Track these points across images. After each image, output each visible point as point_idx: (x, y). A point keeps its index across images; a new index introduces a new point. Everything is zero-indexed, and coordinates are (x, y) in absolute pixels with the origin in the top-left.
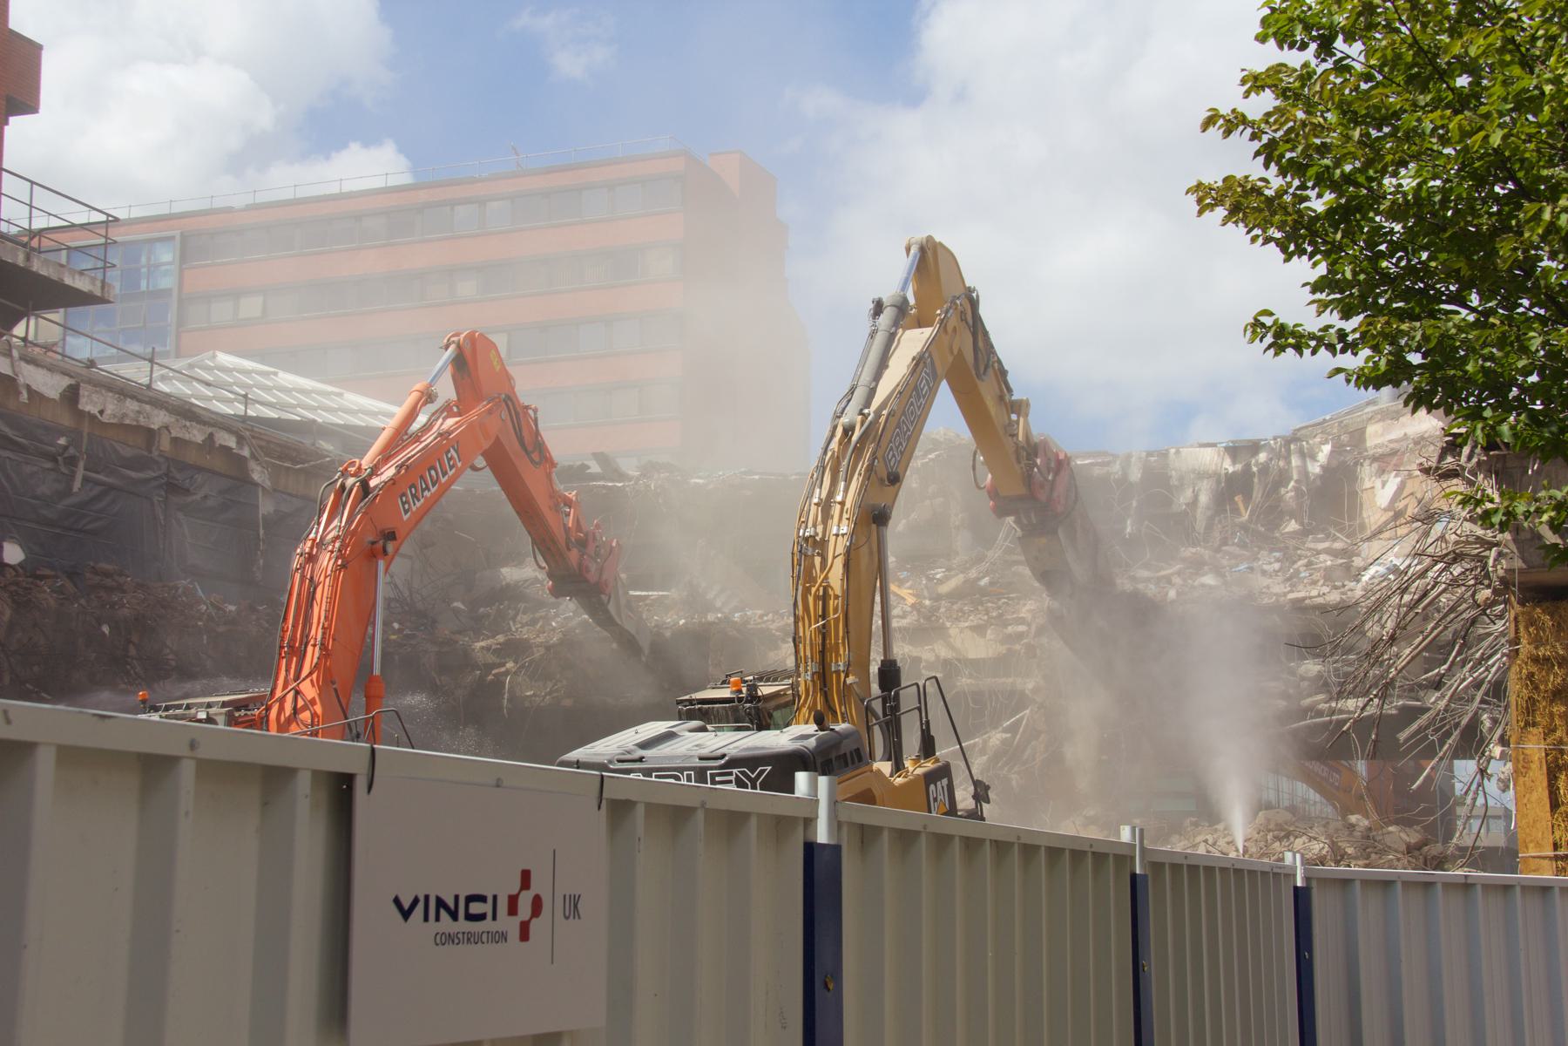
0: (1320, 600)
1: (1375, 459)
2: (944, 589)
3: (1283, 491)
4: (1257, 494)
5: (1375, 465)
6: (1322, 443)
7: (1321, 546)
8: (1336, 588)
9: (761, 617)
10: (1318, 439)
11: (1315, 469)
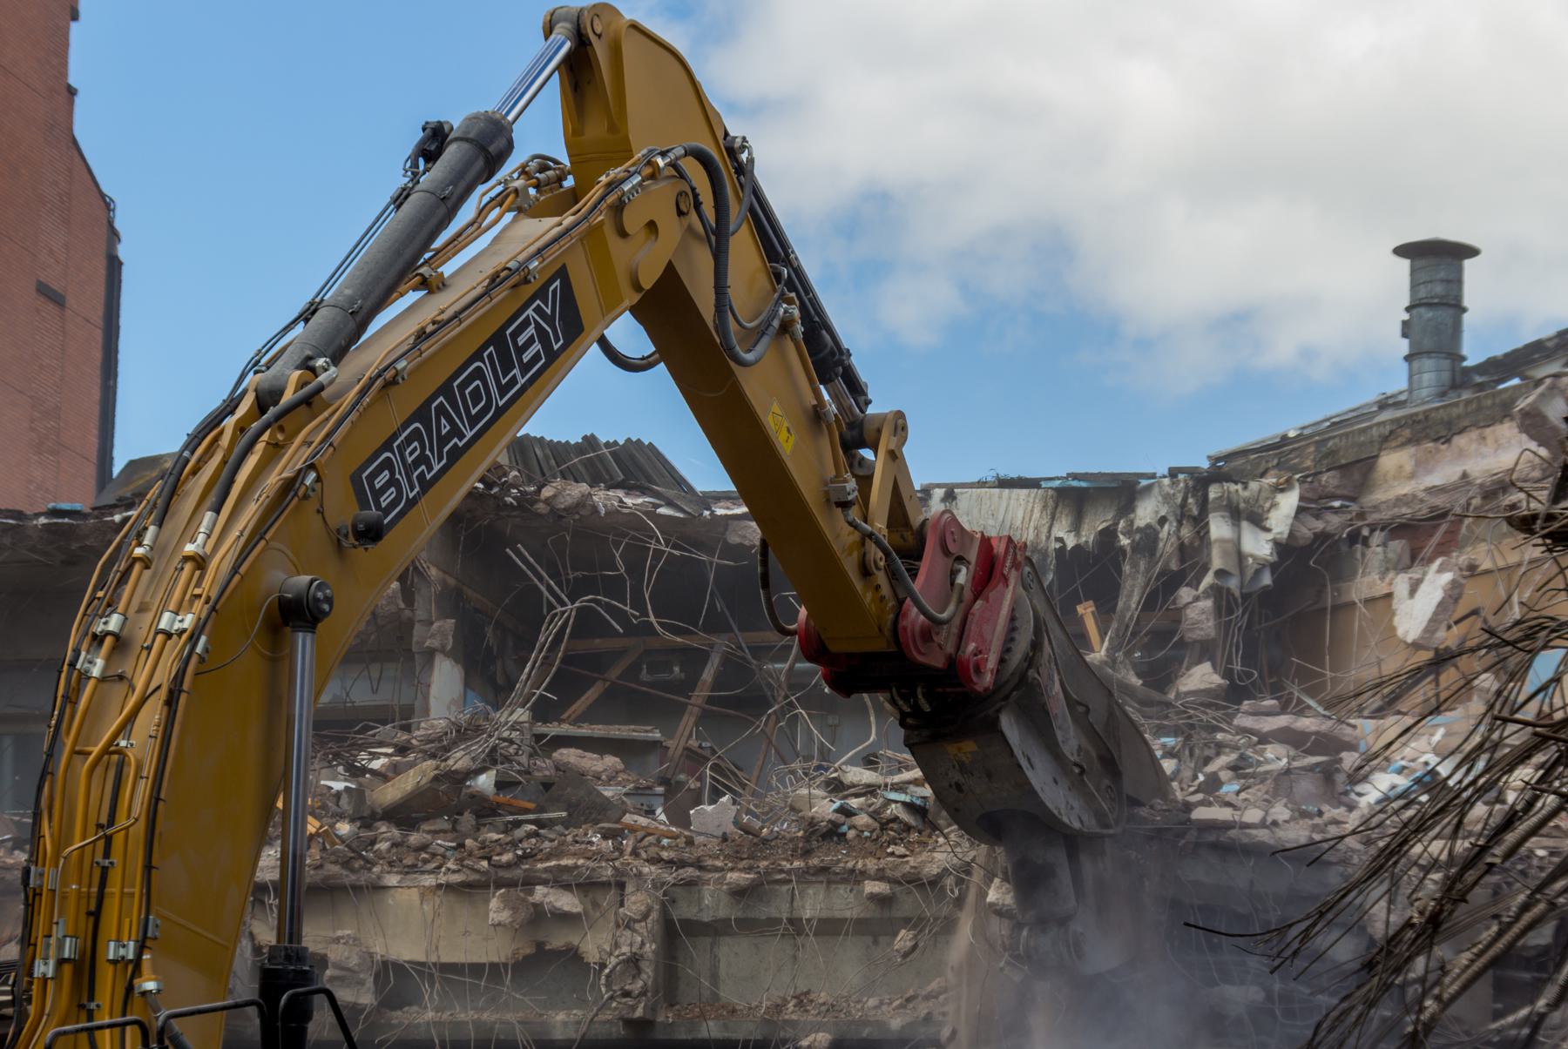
0: (1263, 835)
2: (390, 793)
3: (1185, 594)
4: (1131, 596)
5: (1397, 546)
6: (1279, 489)
7: (1270, 724)
8: (1305, 815)
10: (1270, 480)
11: (1258, 546)
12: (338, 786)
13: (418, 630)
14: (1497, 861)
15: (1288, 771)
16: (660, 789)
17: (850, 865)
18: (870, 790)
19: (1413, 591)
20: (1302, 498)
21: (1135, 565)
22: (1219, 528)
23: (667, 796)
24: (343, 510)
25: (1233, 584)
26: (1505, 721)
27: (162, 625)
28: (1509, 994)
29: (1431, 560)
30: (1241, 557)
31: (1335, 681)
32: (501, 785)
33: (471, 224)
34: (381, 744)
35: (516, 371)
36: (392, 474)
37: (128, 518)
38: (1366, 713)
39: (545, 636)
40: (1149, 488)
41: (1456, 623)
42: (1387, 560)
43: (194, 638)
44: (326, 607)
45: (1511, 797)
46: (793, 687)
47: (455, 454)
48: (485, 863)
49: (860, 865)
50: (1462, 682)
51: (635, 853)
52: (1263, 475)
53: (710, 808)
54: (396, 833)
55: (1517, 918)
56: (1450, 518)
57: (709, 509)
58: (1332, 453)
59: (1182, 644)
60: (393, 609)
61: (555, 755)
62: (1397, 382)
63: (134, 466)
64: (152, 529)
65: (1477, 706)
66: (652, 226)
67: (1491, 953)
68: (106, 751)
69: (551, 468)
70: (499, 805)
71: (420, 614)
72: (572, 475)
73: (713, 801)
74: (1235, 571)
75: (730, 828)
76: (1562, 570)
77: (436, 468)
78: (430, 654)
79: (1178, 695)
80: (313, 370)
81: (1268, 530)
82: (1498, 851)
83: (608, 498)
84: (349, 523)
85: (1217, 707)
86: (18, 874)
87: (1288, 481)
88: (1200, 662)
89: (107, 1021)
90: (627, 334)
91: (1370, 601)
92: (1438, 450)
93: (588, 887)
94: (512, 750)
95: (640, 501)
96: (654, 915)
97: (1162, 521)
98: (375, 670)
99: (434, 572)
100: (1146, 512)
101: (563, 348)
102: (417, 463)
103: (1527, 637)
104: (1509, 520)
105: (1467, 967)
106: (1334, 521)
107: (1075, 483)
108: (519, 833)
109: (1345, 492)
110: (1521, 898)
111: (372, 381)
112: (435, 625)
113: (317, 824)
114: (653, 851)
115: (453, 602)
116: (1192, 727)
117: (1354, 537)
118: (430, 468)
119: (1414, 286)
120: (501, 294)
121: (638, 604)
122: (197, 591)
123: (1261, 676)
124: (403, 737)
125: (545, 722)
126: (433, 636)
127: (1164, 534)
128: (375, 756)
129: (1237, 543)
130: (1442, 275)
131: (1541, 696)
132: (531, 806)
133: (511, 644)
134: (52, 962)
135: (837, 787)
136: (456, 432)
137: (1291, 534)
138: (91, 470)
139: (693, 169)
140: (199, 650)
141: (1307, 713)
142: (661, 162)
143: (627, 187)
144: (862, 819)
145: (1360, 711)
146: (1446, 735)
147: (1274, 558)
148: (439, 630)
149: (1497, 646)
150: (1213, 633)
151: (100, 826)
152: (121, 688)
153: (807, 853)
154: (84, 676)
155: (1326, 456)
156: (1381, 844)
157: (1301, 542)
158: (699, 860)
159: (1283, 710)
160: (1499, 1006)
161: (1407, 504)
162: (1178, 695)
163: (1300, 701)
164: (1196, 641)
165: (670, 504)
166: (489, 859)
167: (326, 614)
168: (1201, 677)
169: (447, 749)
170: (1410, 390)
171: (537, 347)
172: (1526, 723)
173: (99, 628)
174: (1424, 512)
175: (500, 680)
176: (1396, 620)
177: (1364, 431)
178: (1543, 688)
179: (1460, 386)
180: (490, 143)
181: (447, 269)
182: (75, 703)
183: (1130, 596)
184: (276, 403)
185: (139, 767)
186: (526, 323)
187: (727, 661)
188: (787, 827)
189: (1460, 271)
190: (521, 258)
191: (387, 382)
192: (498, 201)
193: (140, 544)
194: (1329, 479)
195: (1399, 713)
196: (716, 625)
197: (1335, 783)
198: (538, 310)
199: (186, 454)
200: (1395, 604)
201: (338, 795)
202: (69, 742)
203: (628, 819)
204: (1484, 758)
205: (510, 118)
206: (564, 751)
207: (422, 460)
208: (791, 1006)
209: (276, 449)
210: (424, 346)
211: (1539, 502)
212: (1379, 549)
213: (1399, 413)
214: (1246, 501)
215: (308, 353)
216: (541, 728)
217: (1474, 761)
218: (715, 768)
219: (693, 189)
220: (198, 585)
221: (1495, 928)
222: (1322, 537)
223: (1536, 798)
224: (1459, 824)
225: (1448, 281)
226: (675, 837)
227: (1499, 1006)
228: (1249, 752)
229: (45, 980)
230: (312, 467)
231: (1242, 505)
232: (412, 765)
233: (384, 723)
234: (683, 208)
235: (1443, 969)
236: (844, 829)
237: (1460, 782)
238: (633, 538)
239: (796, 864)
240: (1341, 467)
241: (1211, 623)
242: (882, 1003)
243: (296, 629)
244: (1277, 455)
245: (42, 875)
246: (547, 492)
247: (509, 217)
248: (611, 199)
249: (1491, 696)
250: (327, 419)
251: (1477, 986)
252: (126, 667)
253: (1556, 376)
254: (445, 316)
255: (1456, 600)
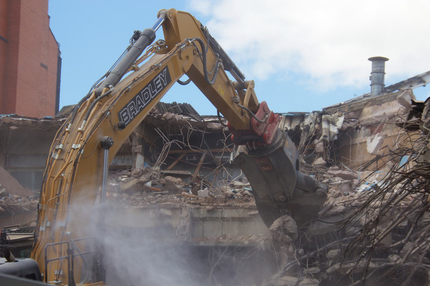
1: (368, 126)
3: (316, 141)
5: (368, 130)
6: (339, 116)
9: (17, 199)
10: (337, 114)
11: (334, 130)
12: (114, 185)
13: (133, 148)
14: (393, 206)
15: (341, 184)
16: (191, 186)
17: (236, 205)
18: (241, 187)
19: (371, 141)
20: (345, 119)
21: (304, 134)
22: (324, 125)
23: (192, 188)
24: (116, 121)
25: (328, 139)
26: (395, 172)
27: (73, 147)
28: (396, 239)
29: (376, 134)
30: (330, 132)
31: (352, 162)
32: (153, 185)
33: (145, 55)
34: (124, 175)
35: (156, 90)
36: (127, 113)
37: (65, 120)
38: (360, 170)
39: (164, 150)
40: (308, 116)
41: (382, 149)
42: (365, 133)
43: (80, 150)
44: (112, 144)
45: (395, 191)
46: (222, 162)
47: (142, 109)
48: (149, 203)
49: (238, 205)
50: (383, 164)
51: (184, 201)
52: (335, 113)
53: (202, 191)
54: (127, 196)
55: (397, 220)
56: (381, 123)
57: (203, 119)
58: (352, 108)
59: (316, 153)
60: (127, 143)
61: (166, 178)
62: (368, 90)
63: (65, 108)
64: (70, 124)
65: (387, 169)
66: (187, 57)
67: (391, 228)
68: (59, 177)
69: (165, 109)
70: (152, 190)
71: (134, 144)
72: (170, 111)
73: (203, 189)
74: (328, 136)
75: (207, 196)
76: (409, 136)
77: (137, 112)
78: (136, 153)
79: (314, 165)
80: (109, 88)
81: (336, 126)
82: (393, 204)
83: (179, 117)
84: (117, 124)
85: (324, 168)
86: (36, 206)
87: (341, 114)
88: (319, 157)
89: (58, 242)
90: (184, 78)
91: (361, 143)
92: (378, 107)
93: (173, 209)
94: (155, 176)
95: (186, 118)
96: (189, 216)
97: (311, 124)
98: (123, 157)
99: (137, 134)
100: (307, 121)
101: (167, 85)
102: (133, 111)
103: (401, 152)
104: (397, 124)
105: (385, 232)
106: (352, 124)
107: (290, 115)
108: (157, 196)
109: (355, 117)
110: (398, 215)
111: (123, 91)
112: (137, 147)
113: (109, 194)
114: (189, 201)
115: (142, 141)
116: (318, 173)
117: (357, 128)
118: (136, 112)
119: (373, 68)
120: (153, 71)
121: (186, 142)
122: (81, 139)
123: (334, 161)
124: (129, 173)
125: (163, 170)
126: (137, 149)
127: (311, 127)
128: (123, 178)
129: (329, 129)
130: (380, 65)
131: (403, 167)
132: (160, 190)
133: (155, 151)
134: (44, 227)
135: (233, 186)
136: (142, 104)
137: (342, 127)
138: (54, 109)
139: (197, 43)
140: (82, 153)
141: (346, 170)
142: (190, 42)
143: (182, 47)
144: (239, 194)
145: (358, 170)
146: (379, 176)
147: (337, 133)
148: (138, 148)
149: (393, 154)
150: (323, 151)
151: (56, 195)
152: (63, 162)
153: (226, 202)
154: (53, 159)
155: (350, 108)
156: (364, 202)
157: (344, 129)
158: (200, 203)
159: (340, 169)
160: (393, 241)
161: (370, 120)
162: (314, 165)
163: (344, 167)
164: (318, 153)
165: (193, 118)
166: (150, 202)
167: (112, 145)
168: (320, 161)
169: (140, 176)
170: (371, 93)
171: (160, 84)
172: (400, 173)
173: (57, 147)
174: (374, 122)
175: (153, 160)
176: (367, 148)
177: (360, 102)
178: (405, 165)
179: (384, 91)
180: (150, 36)
181: (139, 66)
182: (51, 165)
183: (303, 141)
184: (100, 95)
185: (67, 181)
186: (158, 79)
187: (207, 155)
188: (221, 195)
189: (384, 64)
190: (157, 63)
191: (126, 91)
192: (151, 50)
193: (67, 128)
194: (351, 114)
195: (368, 170)
196: (204, 147)
197: (352, 187)
198: (161, 76)
199: (78, 107)
200: (367, 144)
201: (114, 187)
202: (49, 174)
203: (183, 193)
204: (390, 181)
205: (155, 30)
206: (168, 177)
207: (134, 110)
208: (221, 238)
209: (100, 106)
210: (135, 83)
211: (404, 120)
212: (363, 131)
213: (368, 98)
214: (331, 119)
215: (108, 84)
216: (162, 171)
217: (387, 182)
218: (204, 181)
219: (197, 48)
220: (81, 137)
221: (392, 222)
222: (349, 128)
223: (403, 191)
224: (384, 197)
225: (381, 67)
226: (194, 197)
227: (393, 241)
228: (331, 179)
229: (42, 231)
230: (109, 110)
231: (330, 120)
232: (132, 180)
233: (125, 170)
234: (195, 53)
235: (379, 232)
236: (234, 196)
237: (384, 187)
238: (185, 126)
239: (223, 204)
240: (354, 111)
241: (322, 148)
242: (243, 238)
243: (104, 149)
244: (338, 108)
245: (42, 206)
246: (164, 115)
247: (154, 54)
248: (178, 50)
249: (391, 167)
250: (112, 99)
251: (388, 236)
252: (64, 157)
253: (407, 90)
254: (140, 76)
255: (382, 143)
